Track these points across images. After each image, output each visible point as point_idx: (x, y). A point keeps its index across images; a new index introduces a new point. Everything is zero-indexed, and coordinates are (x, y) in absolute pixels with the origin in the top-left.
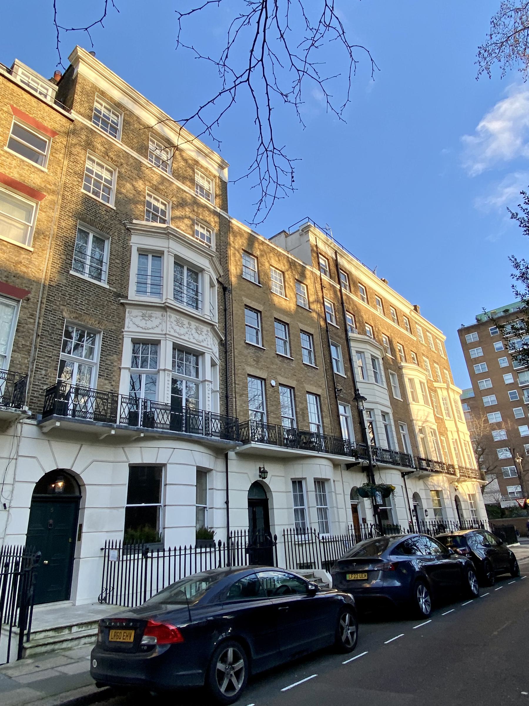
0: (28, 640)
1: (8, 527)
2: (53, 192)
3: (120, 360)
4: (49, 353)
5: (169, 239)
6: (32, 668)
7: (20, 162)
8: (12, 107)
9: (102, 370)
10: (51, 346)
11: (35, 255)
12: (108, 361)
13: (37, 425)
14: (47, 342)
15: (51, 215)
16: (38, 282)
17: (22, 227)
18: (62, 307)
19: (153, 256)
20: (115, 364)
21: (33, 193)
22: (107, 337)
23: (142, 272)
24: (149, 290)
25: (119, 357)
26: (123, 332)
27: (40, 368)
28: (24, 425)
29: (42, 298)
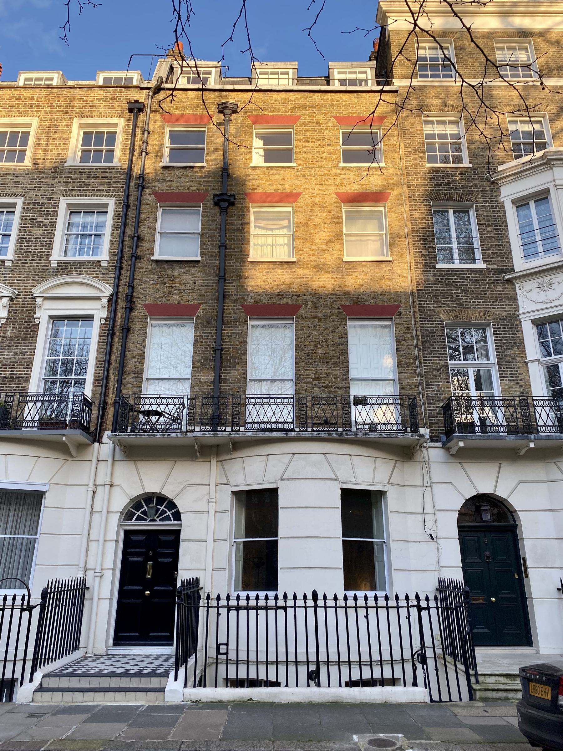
0: (477, 682)
1: (441, 558)
2: (397, 185)
3: (523, 352)
4: (436, 365)
5: (551, 169)
6: (481, 712)
7: (357, 170)
8: (336, 117)
9: (503, 371)
10: (436, 357)
11: (396, 264)
12: (508, 357)
13: (443, 447)
14: (430, 354)
15: (401, 213)
16: (406, 293)
17: (378, 238)
18: (437, 310)
19: (535, 201)
20: (518, 358)
21: (376, 197)
22: (500, 328)
23: (526, 231)
24: (540, 249)
25: (520, 349)
26: (518, 316)
27: (430, 385)
28: (429, 449)
29: (414, 307)
